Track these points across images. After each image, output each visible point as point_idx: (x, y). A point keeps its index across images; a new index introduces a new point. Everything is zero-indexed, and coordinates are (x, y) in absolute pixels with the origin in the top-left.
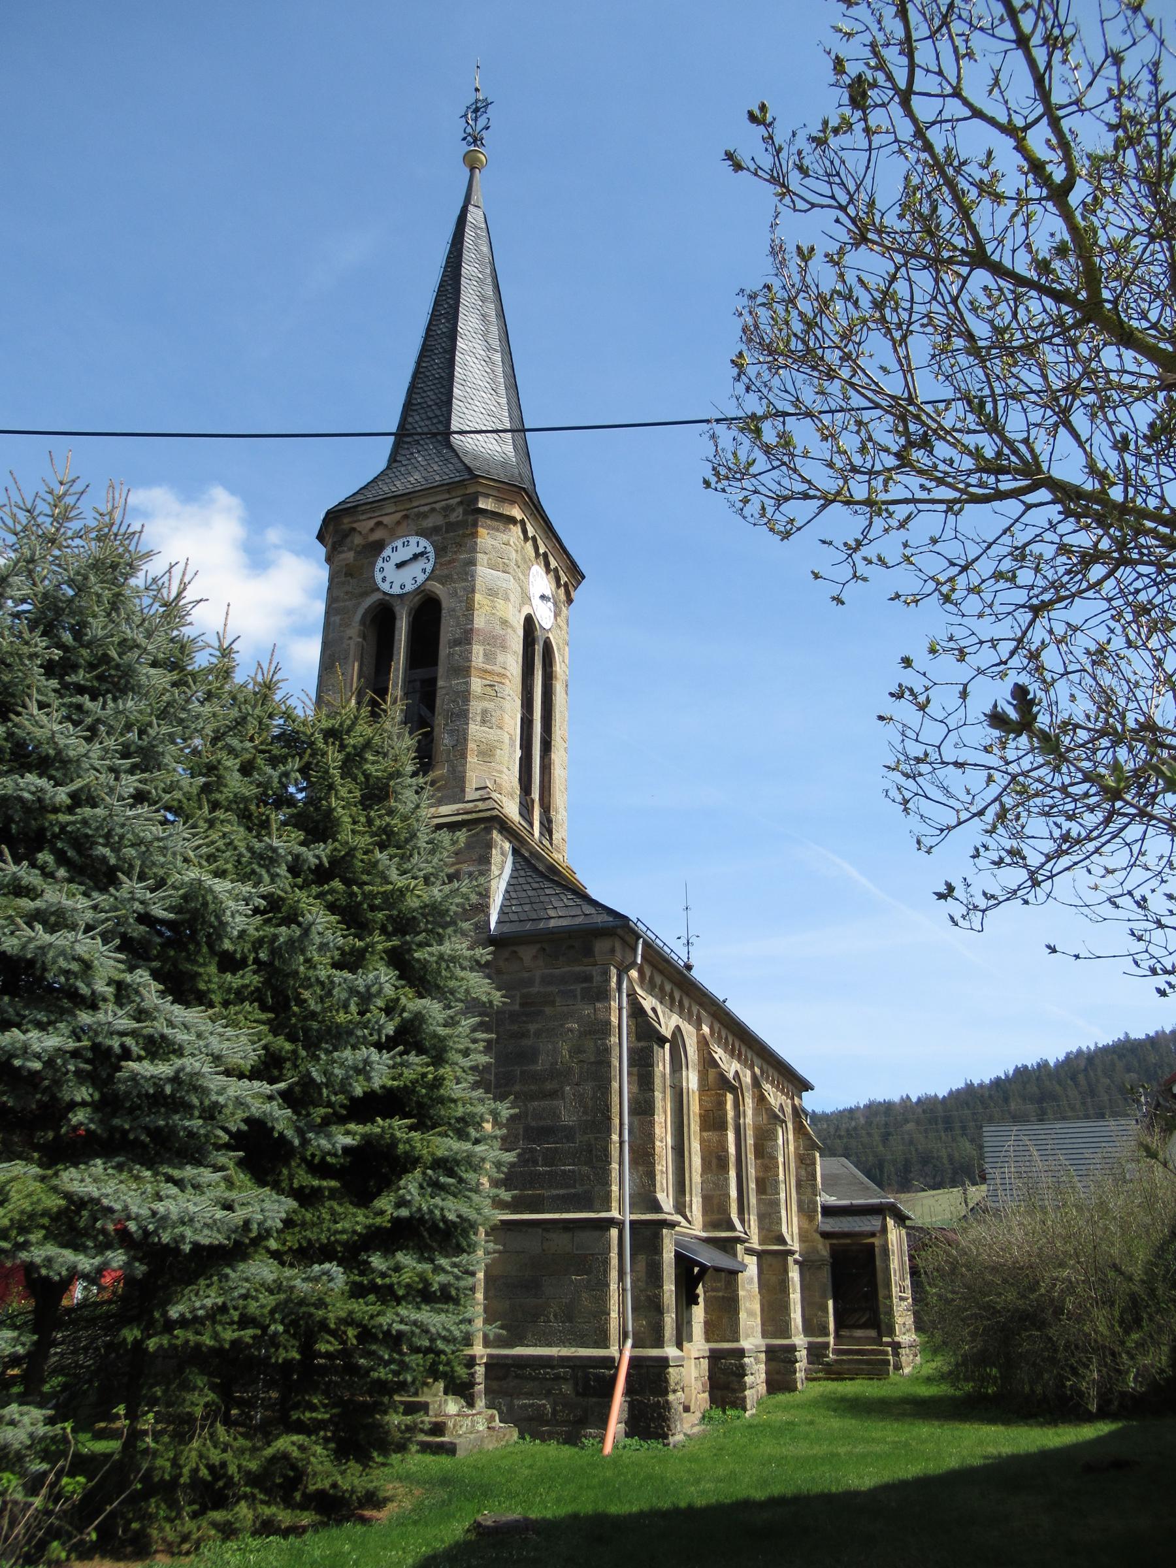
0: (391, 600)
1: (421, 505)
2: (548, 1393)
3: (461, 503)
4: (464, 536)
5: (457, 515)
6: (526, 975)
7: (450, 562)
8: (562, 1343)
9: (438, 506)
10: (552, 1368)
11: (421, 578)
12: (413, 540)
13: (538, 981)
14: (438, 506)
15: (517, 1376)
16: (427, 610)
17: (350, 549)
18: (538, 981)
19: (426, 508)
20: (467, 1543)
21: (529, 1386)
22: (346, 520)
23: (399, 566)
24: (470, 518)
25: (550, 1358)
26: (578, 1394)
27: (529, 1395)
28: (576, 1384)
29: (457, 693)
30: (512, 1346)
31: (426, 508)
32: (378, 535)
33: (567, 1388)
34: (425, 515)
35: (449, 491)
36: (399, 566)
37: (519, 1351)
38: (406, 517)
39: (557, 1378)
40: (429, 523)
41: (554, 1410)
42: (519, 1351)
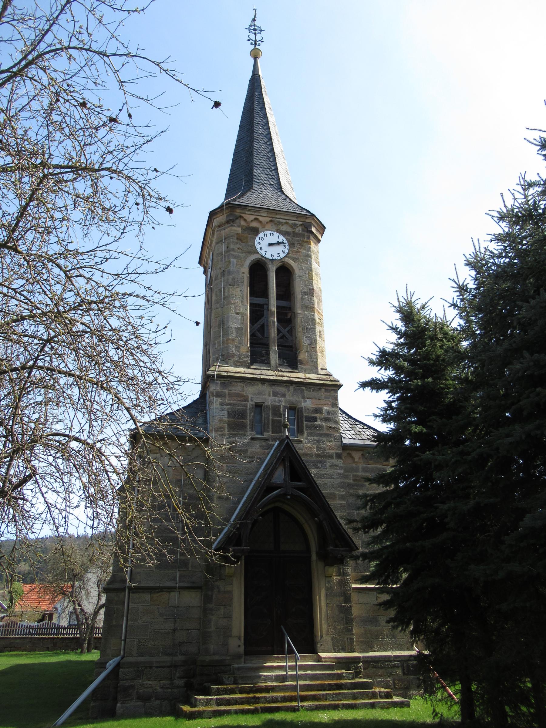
0: (266, 261)
1: (281, 218)
2: (390, 675)
3: (301, 225)
4: (304, 241)
5: (299, 230)
6: (354, 466)
7: (297, 252)
8: (391, 649)
9: (290, 222)
10: (391, 661)
11: (282, 255)
12: (276, 234)
13: (360, 470)
14: (290, 222)
15: (375, 667)
16: (285, 272)
17: (239, 226)
18: (360, 470)
19: (284, 221)
20: (452, 725)
21: (381, 672)
22: (238, 211)
23: (270, 245)
24: (306, 234)
25: (390, 656)
26: (404, 674)
27: (381, 676)
28: (403, 670)
29: (309, 319)
30: (367, 652)
31: (284, 221)
32: (255, 224)
33: (399, 671)
34: (283, 224)
35: (297, 217)
36: (270, 245)
37: (371, 654)
38: (271, 221)
39: (394, 666)
40: (284, 228)
41: (394, 682)
42: (371, 654)
